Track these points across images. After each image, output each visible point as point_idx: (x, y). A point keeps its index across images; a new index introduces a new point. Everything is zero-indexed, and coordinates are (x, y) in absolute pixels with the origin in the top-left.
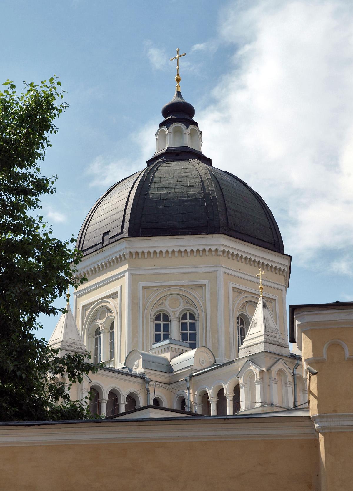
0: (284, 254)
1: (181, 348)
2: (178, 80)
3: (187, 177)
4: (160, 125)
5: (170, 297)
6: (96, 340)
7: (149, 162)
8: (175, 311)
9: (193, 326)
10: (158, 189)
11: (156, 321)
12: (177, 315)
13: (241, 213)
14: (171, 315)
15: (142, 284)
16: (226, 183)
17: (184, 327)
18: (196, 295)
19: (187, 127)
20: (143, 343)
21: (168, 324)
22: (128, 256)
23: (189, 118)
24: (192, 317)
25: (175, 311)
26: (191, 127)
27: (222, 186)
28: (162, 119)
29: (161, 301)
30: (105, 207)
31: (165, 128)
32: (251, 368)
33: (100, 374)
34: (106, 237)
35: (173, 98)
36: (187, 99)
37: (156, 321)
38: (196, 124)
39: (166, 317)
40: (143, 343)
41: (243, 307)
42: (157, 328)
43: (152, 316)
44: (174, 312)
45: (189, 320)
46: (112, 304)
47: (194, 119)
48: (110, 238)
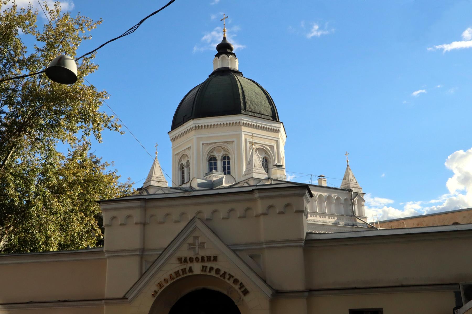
0: (279, 122)
1: (163, 288)
7: (209, 76)
8: (219, 156)
9: (229, 163)
12: (220, 158)
14: (217, 158)
15: (201, 143)
17: (224, 163)
18: (229, 147)
19: (228, 56)
22: (194, 128)
24: (228, 158)
25: (219, 156)
29: (212, 151)
39: (215, 159)
41: (241, 283)
42: (210, 164)
44: (219, 156)
45: (226, 160)
46: (187, 152)
47: (233, 52)
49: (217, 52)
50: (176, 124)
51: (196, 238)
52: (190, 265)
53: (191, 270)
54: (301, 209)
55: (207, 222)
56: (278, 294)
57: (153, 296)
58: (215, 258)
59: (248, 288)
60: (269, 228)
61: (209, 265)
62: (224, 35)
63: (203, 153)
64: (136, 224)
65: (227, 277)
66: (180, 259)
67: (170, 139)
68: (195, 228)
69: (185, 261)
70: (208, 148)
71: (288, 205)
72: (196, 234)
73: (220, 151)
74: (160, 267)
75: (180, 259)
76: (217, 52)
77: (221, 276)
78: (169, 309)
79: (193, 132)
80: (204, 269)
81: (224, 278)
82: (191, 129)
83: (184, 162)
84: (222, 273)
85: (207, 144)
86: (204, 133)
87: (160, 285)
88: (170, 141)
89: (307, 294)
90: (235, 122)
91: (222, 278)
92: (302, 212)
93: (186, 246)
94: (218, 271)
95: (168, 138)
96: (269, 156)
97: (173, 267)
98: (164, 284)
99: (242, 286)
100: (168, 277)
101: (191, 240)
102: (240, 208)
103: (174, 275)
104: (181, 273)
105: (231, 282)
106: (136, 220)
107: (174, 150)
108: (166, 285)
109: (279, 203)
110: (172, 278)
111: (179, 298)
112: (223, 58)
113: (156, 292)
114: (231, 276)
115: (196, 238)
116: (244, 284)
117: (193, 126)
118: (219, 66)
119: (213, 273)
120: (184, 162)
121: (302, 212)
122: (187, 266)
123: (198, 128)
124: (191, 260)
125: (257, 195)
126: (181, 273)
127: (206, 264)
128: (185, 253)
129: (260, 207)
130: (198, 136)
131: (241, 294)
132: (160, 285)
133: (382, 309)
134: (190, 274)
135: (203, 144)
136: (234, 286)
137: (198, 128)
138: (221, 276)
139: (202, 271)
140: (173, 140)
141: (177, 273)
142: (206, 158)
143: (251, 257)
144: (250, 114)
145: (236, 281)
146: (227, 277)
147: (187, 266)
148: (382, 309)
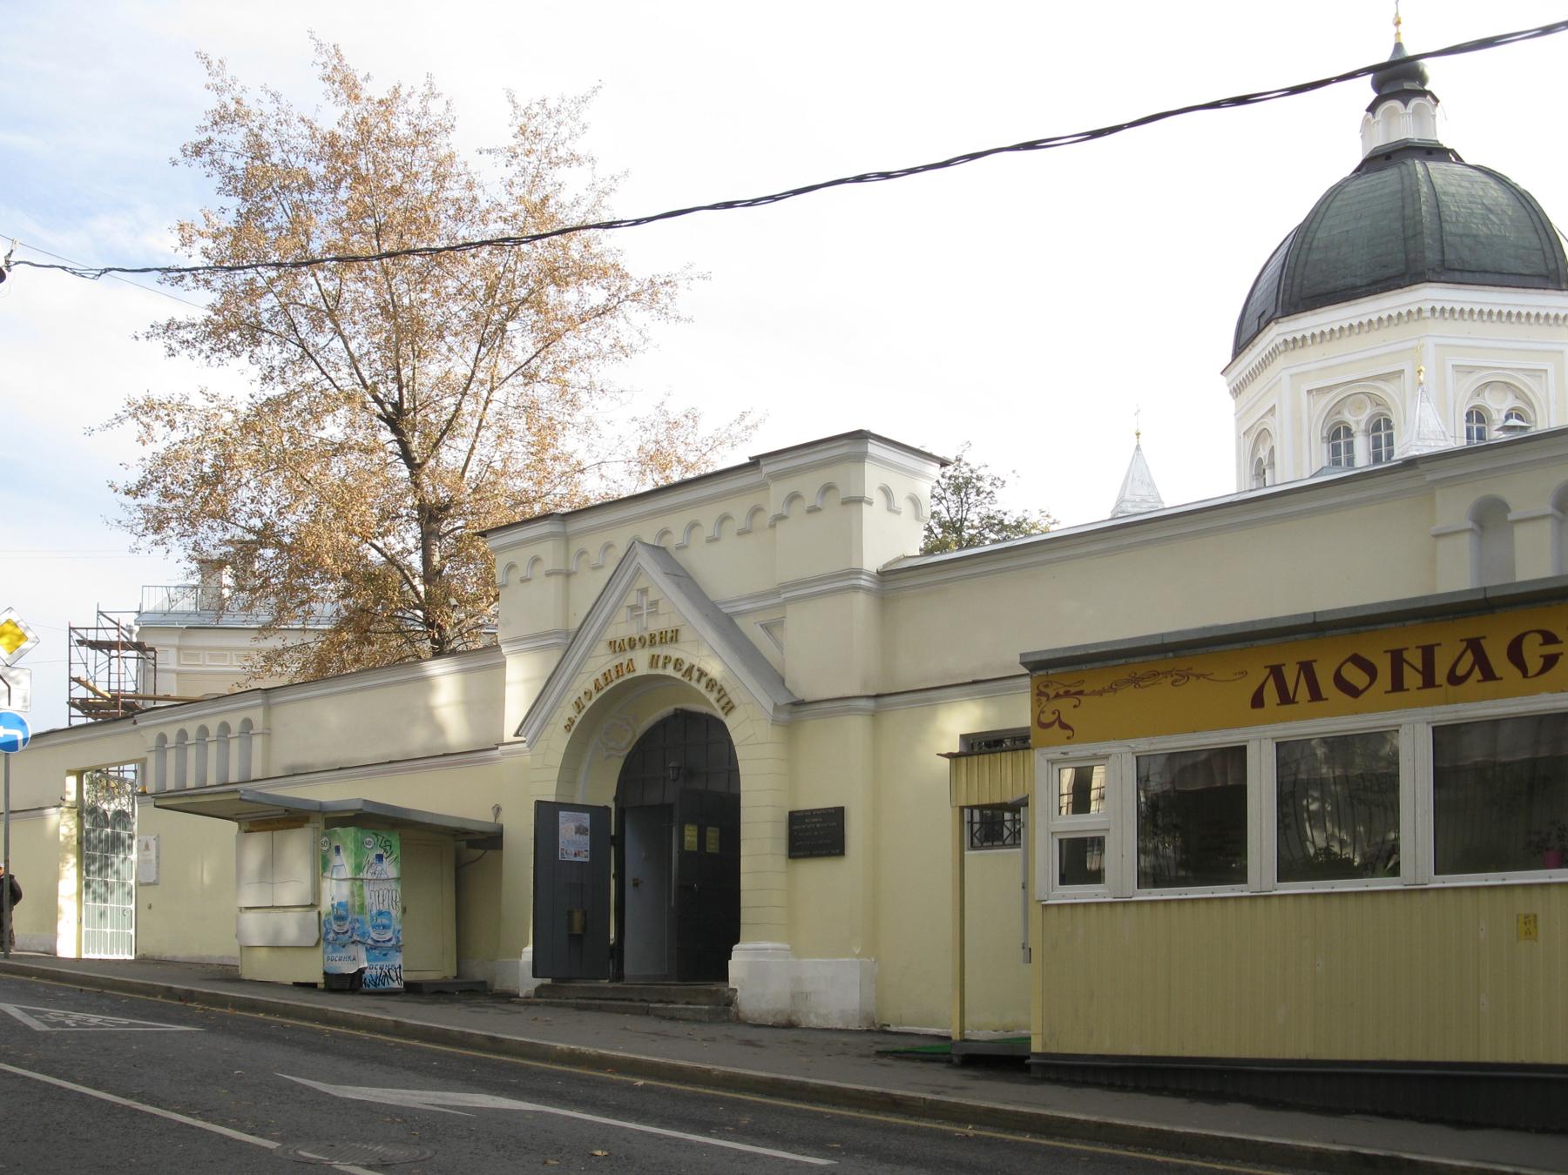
2: (1398, 23)
8: (1358, 420)
12: (1363, 426)
14: (1354, 428)
17: (1377, 445)
18: (1389, 390)
22: (1282, 348)
25: (1358, 420)
29: (1337, 408)
39: (1349, 432)
42: (1335, 450)
44: (1358, 423)
47: (1427, 87)
49: (1374, 95)
50: (1241, 345)
51: (644, 591)
52: (629, 655)
53: (630, 666)
54: (854, 494)
55: (659, 551)
56: (798, 707)
57: (568, 728)
59: (734, 697)
60: (797, 550)
61: (661, 651)
62: (1398, 34)
63: (1310, 418)
64: (549, 574)
65: (695, 674)
66: (612, 644)
67: (1227, 390)
68: (638, 570)
70: (1326, 401)
71: (828, 488)
72: (642, 583)
73: (1360, 408)
74: (578, 666)
75: (612, 644)
76: (1374, 95)
78: (617, 766)
79: (1280, 361)
80: (654, 661)
82: (1274, 353)
83: (1263, 453)
84: (685, 667)
85: (1320, 390)
86: (1310, 358)
89: (870, 704)
90: (1404, 312)
91: (686, 680)
92: (859, 500)
93: (623, 614)
94: (678, 664)
95: (1222, 386)
96: (1531, 405)
97: (601, 662)
100: (592, 687)
101: (632, 599)
102: (739, 509)
103: (602, 682)
105: (701, 687)
106: (549, 564)
108: (589, 705)
109: (809, 485)
110: (598, 689)
111: (638, 736)
112: (1392, 113)
113: (571, 721)
114: (702, 674)
115: (644, 591)
116: (728, 689)
117: (1280, 340)
118: (1380, 140)
119: (670, 671)
120: (1263, 453)
121: (859, 500)
122: (623, 659)
123: (1295, 344)
124: (632, 644)
125: (767, 469)
127: (657, 651)
128: (622, 629)
130: (1294, 371)
132: (579, 706)
134: (630, 676)
135: (1309, 392)
137: (1295, 344)
139: (651, 666)
140: (1236, 391)
143: (766, 627)
144: (1457, 275)
146: (695, 674)
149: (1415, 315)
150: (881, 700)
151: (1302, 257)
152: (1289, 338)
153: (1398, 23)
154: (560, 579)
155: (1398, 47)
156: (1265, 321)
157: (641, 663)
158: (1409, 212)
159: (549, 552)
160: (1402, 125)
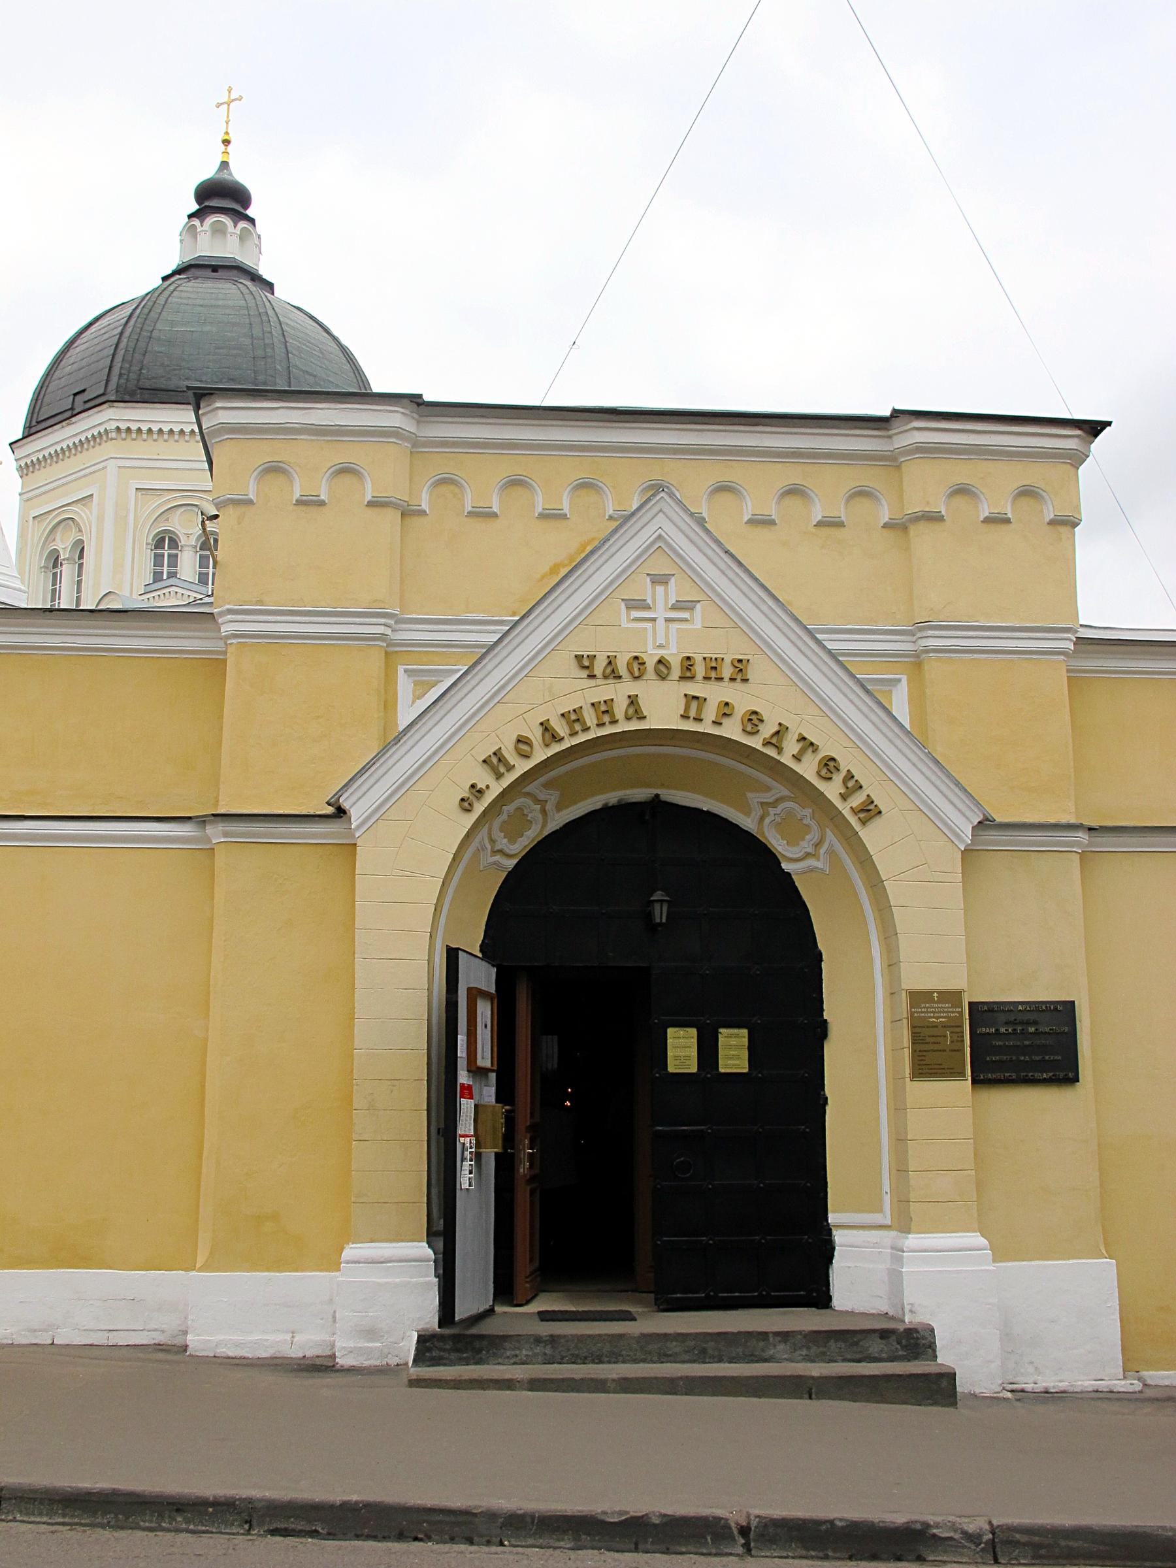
2: (226, 142)
3: (226, 307)
4: (190, 216)
5: (182, 509)
6: (55, 575)
7: (165, 279)
10: (173, 323)
11: (156, 548)
13: (315, 376)
14: (183, 541)
16: (292, 324)
20: (132, 584)
21: (177, 556)
23: (242, 210)
26: (243, 224)
27: (285, 327)
28: (195, 207)
30: (78, 349)
31: (196, 222)
32: (749, 820)
33: (379, 813)
34: (79, 398)
35: (208, 172)
36: (240, 174)
37: (156, 548)
38: (252, 221)
39: (174, 543)
40: (132, 584)
41: (850, 776)
43: (150, 541)
46: (78, 512)
47: (250, 212)
48: (85, 402)
50: (38, 422)
52: (627, 687)
53: (634, 707)
57: (465, 805)
58: (740, 671)
59: (873, 789)
60: (954, 577)
61: (715, 694)
66: (585, 663)
67: (14, 465)
69: (613, 674)
70: (156, 504)
75: (585, 663)
77: (767, 743)
79: (107, 449)
81: (780, 750)
83: (63, 544)
87: (496, 763)
88: (17, 475)
94: (753, 720)
98: (512, 759)
99: (852, 785)
104: (590, 718)
107: (27, 498)
108: (522, 767)
109: (997, 487)
114: (807, 745)
119: (732, 730)
120: (63, 544)
122: (618, 693)
126: (590, 718)
129: (925, 486)
131: (853, 820)
133: (1066, 1011)
134: (635, 725)
136: (821, 786)
138: (767, 743)
140: (25, 470)
141: (574, 719)
142: (147, 536)
145: (829, 765)
147: (618, 693)
148: (1066, 1011)
149: (101, 437)
150: (1099, 839)
151: (142, 344)
152: (123, 426)
153: (226, 142)
154: (391, 517)
155: (225, 165)
156: (82, 402)
157: (663, 709)
158: (257, 332)
159: (385, 473)
160: (219, 241)
